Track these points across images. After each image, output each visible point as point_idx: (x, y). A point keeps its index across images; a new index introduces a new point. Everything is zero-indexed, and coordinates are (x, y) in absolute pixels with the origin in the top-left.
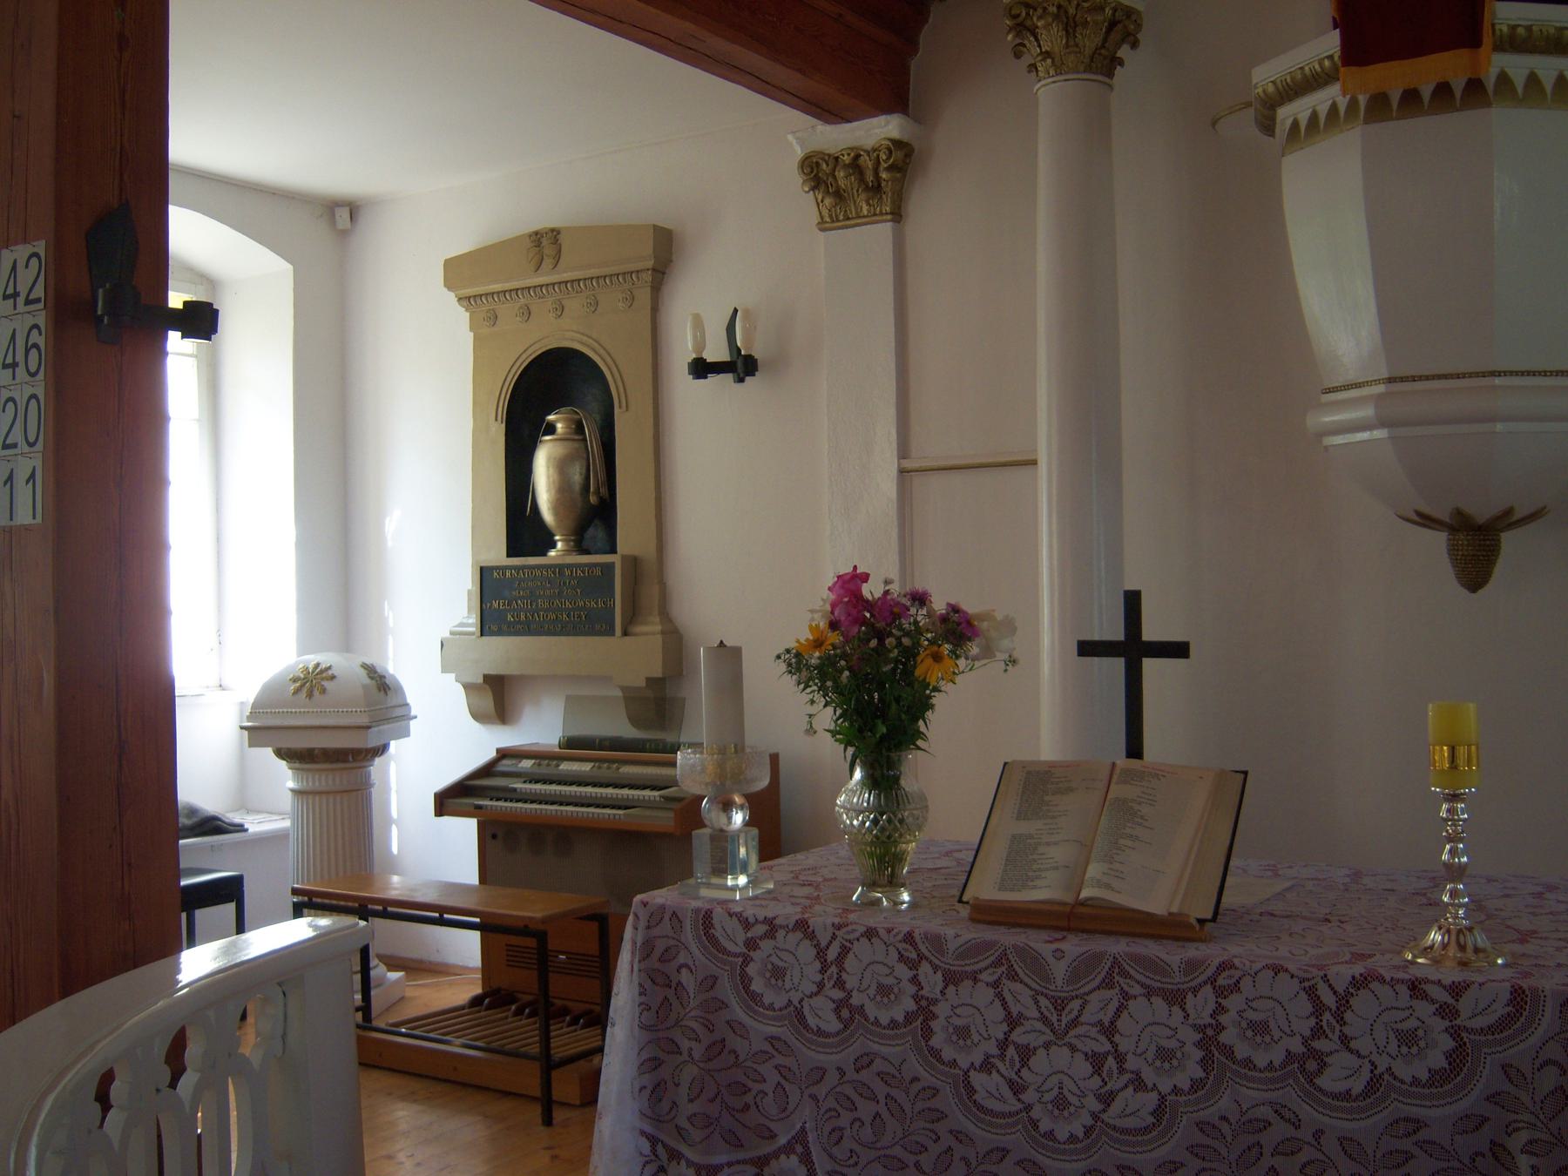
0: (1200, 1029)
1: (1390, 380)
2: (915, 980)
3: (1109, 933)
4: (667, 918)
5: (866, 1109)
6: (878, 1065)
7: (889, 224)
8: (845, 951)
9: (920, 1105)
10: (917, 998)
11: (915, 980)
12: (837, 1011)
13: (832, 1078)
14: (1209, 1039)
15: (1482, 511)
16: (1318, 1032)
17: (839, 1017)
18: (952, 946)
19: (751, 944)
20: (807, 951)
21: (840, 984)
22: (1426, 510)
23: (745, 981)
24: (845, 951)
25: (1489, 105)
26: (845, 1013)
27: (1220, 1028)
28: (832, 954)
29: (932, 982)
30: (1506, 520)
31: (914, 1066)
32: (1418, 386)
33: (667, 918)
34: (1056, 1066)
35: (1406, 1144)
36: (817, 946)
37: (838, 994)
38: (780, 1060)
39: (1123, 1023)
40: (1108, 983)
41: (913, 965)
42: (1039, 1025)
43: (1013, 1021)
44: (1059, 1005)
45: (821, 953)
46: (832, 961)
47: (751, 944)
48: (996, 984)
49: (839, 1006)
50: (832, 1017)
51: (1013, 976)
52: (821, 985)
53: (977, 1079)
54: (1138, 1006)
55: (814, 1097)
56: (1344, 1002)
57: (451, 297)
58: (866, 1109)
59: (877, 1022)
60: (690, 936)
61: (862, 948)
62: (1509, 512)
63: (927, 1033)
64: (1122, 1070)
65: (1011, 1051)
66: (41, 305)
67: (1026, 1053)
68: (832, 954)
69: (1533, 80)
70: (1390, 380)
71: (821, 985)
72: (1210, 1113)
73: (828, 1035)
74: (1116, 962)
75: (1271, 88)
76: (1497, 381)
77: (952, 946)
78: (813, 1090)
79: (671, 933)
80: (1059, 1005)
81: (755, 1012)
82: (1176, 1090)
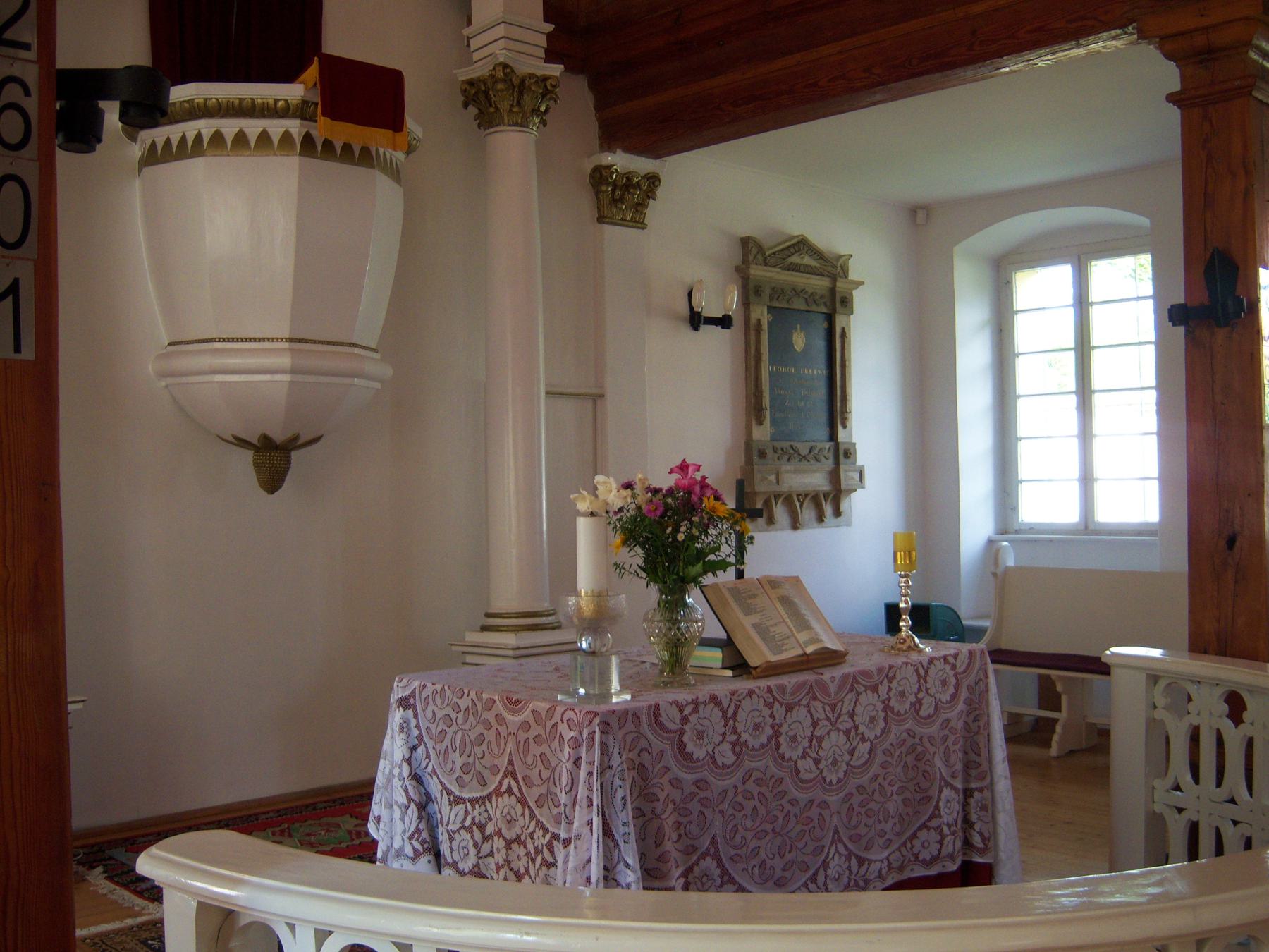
0: (883, 702)
1: (291, 340)
2: (772, 716)
3: (784, 673)
4: (630, 717)
5: (749, 805)
6: (756, 775)
7: (286, 171)
8: (737, 707)
9: (775, 792)
10: (772, 726)
11: (772, 716)
12: (733, 749)
13: (730, 794)
14: (887, 708)
15: (279, 436)
16: (919, 689)
17: (734, 753)
18: (789, 688)
19: (685, 720)
20: (717, 713)
21: (735, 730)
22: (243, 436)
23: (681, 746)
24: (737, 707)
25: (372, 167)
26: (737, 749)
27: (889, 699)
28: (730, 713)
29: (779, 710)
30: (293, 444)
31: (773, 769)
32: (267, 345)
33: (630, 717)
34: (835, 742)
35: (946, 732)
36: (722, 710)
37: (734, 738)
38: (702, 794)
39: (859, 709)
40: (851, 690)
41: (770, 706)
42: (826, 723)
43: (815, 724)
44: (833, 707)
45: (724, 713)
46: (730, 717)
47: (685, 720)
48: (807, 706)
49: (734, 744)
50: (730, 754)
51: (815, 698)
52: (724, 735)
53: (801, 764)
54: (863, 698)
55: (721, 812)
56: (926, 672)
57: (98, 146)
58: (749, 805)
59: (753, 749)
60: (645, 726)
61: (746, 704)
62: (296, 438)
63: (778, 745)
64: (857, 734)
65: (814, 742)
66: (32, 55)
67: (820, 740)
68: (730, 713)
69: (264, 137)
70: (291, 340)
71: (724, 735)
72: (886, 745)
73: (729, 767)
74: (854, 677)
75: (210, 103)
76: (357, 350)
77: (789, 688)
78: (721, 807)
79: (634, 728)
80: (833, 707)
81: (698, 767)
82: (876, 737)
